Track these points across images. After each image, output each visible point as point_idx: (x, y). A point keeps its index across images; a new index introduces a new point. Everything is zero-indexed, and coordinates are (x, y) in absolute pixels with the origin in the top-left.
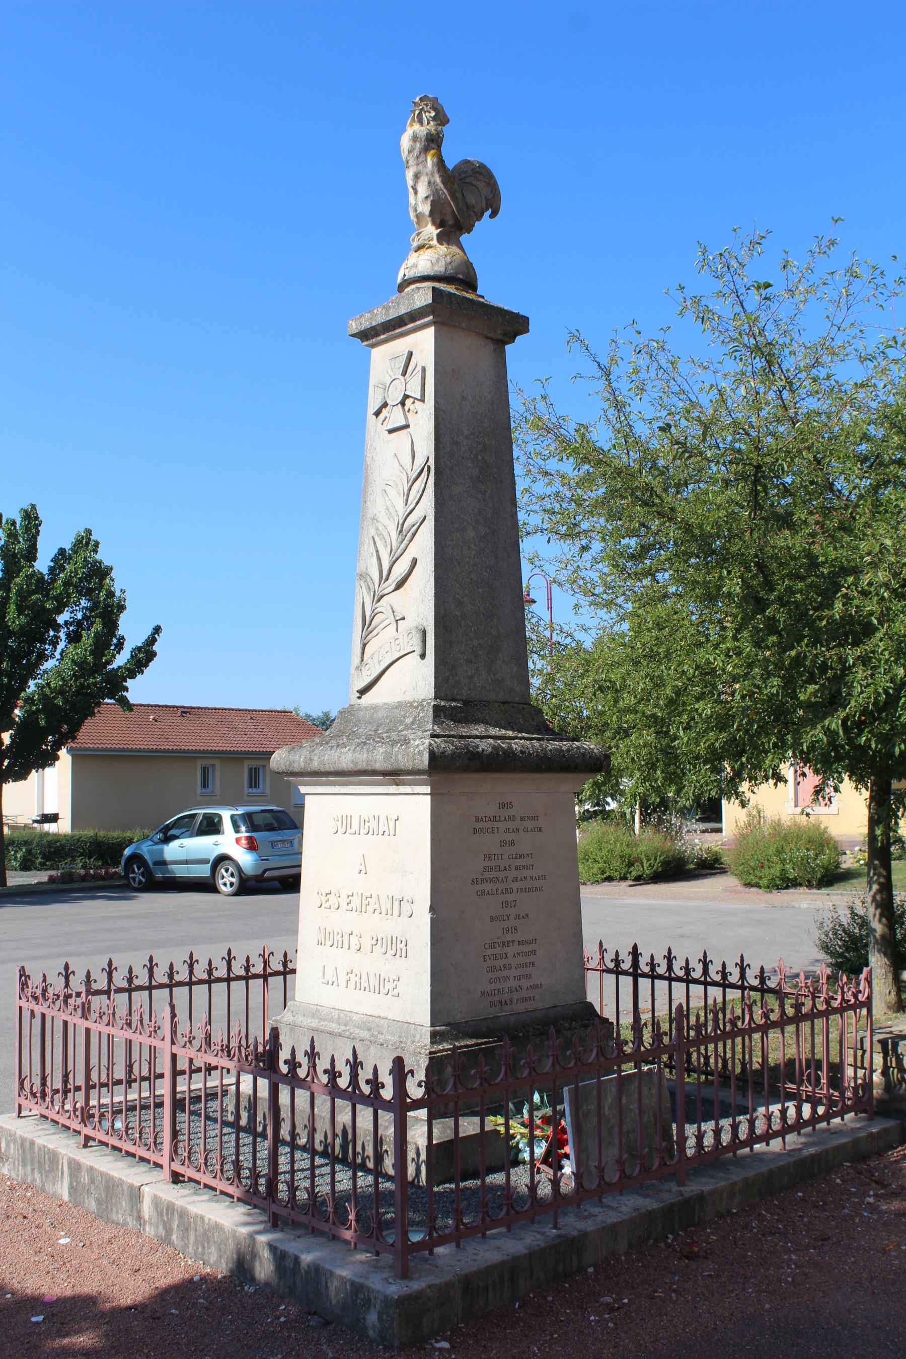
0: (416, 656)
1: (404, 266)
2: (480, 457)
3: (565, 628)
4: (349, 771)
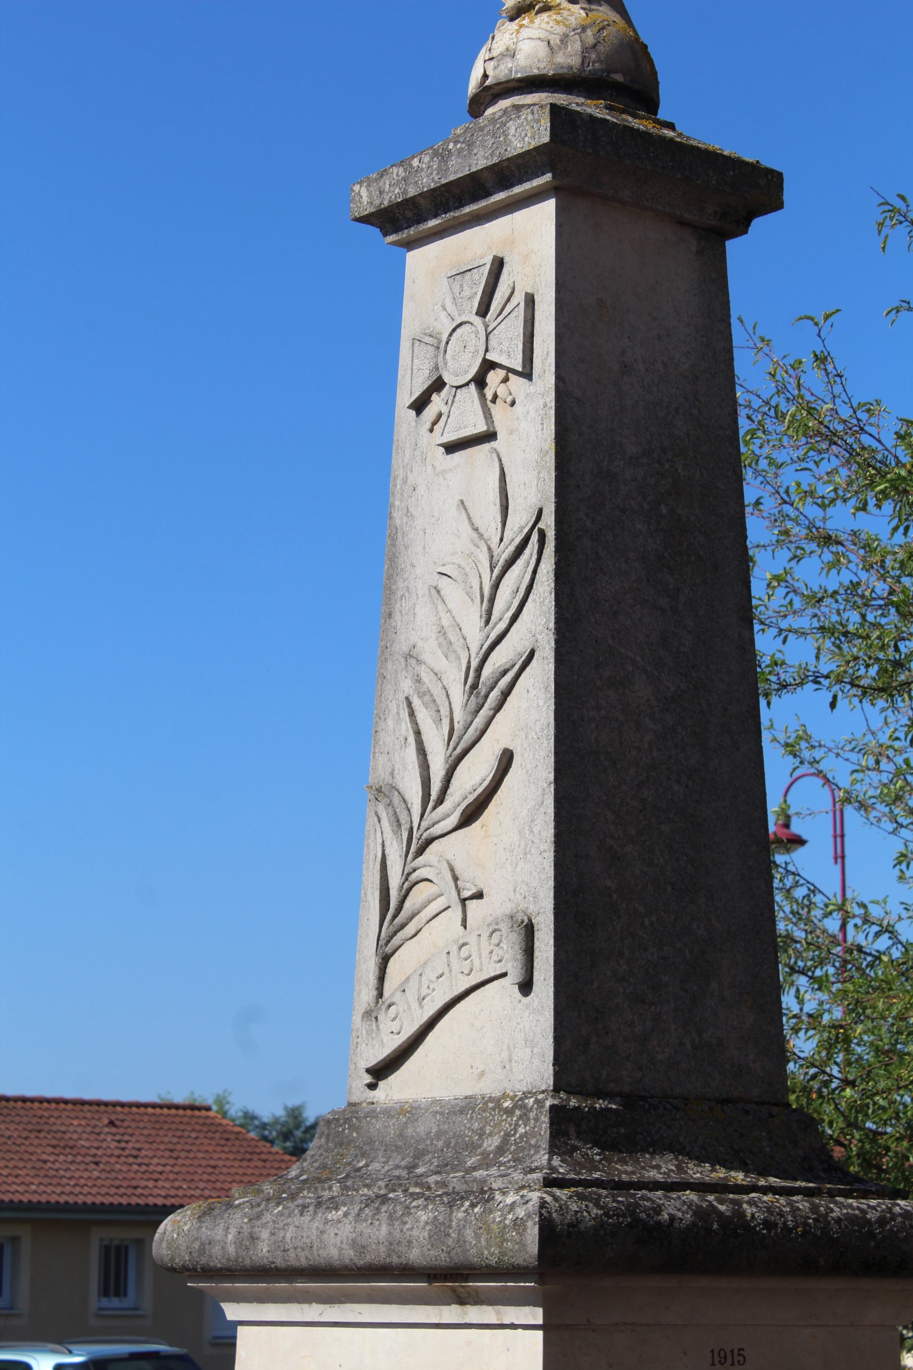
0: (509, 986)
1: (483, 54)
2: (664, 509)
3: (875, 912)
4: (346, 1268)
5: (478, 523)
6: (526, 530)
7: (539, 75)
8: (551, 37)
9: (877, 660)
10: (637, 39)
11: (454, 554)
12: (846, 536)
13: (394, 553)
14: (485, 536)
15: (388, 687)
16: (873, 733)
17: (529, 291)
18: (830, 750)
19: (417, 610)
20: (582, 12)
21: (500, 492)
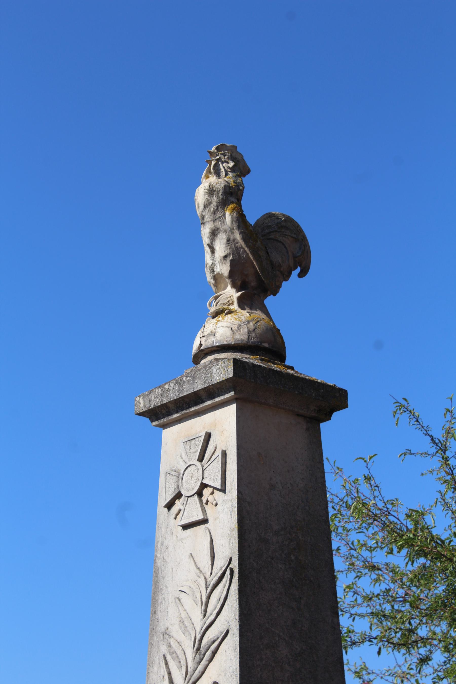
1: (200, 334)
2: (293, 557)
5: (199, 565)
6: (224, 569)
7: (227, 344)
8: (233, 326)
9: (401, 629)
10: (275, 327)
11: (187, 581)
12: (383, 566)
13: (157, 581)
14: (203, 572)
15: (154, 650)
16: (399, 666)
17: (224, 449)
18: (378, 675)
19: (169, 610)
20: (248, 314)
21: (211, 550)
